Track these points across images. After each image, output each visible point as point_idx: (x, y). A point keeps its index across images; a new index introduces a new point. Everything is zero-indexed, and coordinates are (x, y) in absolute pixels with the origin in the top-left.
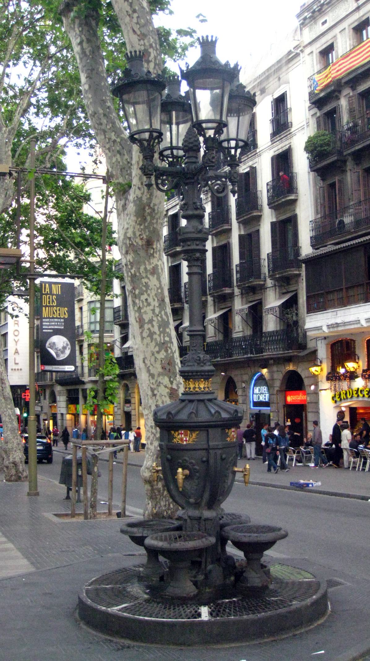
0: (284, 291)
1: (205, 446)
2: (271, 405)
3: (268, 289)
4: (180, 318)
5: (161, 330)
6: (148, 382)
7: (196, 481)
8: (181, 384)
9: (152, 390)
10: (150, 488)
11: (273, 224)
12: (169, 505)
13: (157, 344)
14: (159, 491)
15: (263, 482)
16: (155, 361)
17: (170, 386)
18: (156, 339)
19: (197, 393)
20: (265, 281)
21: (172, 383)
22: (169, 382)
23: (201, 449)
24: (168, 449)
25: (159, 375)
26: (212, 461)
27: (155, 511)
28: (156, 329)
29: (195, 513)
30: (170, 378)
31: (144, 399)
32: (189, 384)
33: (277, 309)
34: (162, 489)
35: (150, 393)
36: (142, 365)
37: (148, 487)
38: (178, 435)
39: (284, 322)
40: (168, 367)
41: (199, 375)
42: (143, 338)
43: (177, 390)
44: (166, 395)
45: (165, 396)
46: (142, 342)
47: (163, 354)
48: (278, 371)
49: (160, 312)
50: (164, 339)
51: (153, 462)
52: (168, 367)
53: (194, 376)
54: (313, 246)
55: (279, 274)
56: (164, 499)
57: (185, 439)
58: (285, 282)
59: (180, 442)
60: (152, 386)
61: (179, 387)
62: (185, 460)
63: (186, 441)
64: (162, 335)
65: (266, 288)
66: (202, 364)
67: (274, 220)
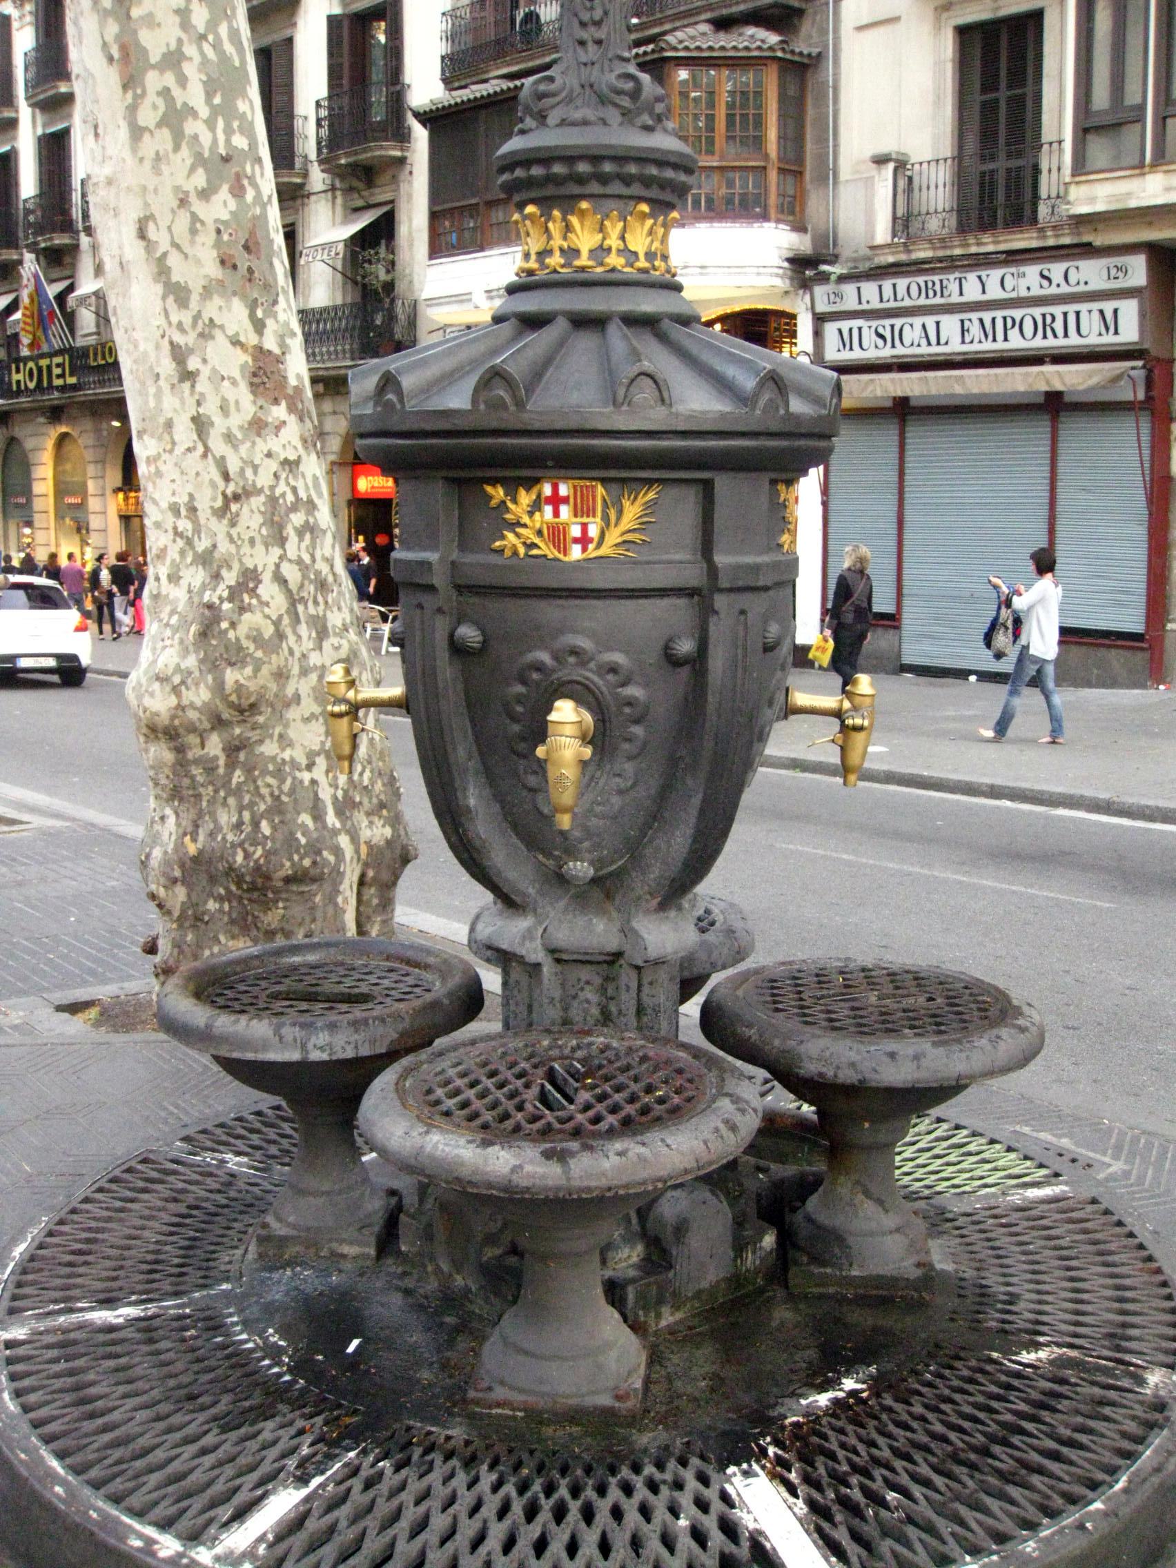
0: (360, 203)
1: (693, 575)
3: (313, 198)
4: (68, 273)
5: (217, 100)
6: (161, 321)
7: (629, 767)
8: (294, 334)
9: (179, 355)
10: (169, 757)
11: (333, 21)
12: (256, 825)
13: (199, 160)
14: (210, 770)
15: (967, 778)
16: (193, 232)
17: (252, 339)
18: (195, 137)
19: (612, 282)
20: (305, 175)
21: (259, 326)
22: (250, 328)
23: (663, 593)
24: (459, 588)
25: (207, 292)
26: (717, 662)
27: (192, 849)
28: (195, 95)
29: (596, 931)
30: (253, 306)
31: (143, 393)
32: (568, 228)
33: (341, 247)
34: (222, 762)
35: (167, 367)
36: (134, 251)
37: (161, 752)
38: (536, 507)
39: (355, 283)
40: (244, 261)
41: (627, 180)
42: (137, 132)
43: (279, 360)
44: (236, 374)
45: (234, 383)
46: (134, 150)
47: (221, 207)
48: (335, 413)
49: (212, 25)
50: (228, 141)
51: (185, 652)
52: (244, 261)
53: (604, 179)
54: (447, 81)
55: (347, 155)
56: (232, 801)
57: (576, 531)
58: (362, 177)
59: (546, 549)
60: (179, 339)
61: (285, 349)
62: (575, 652)
63: (584, 540)
64: (220, 124)
65: (308, 196)
66: (647, 119)
67: (337, 10)
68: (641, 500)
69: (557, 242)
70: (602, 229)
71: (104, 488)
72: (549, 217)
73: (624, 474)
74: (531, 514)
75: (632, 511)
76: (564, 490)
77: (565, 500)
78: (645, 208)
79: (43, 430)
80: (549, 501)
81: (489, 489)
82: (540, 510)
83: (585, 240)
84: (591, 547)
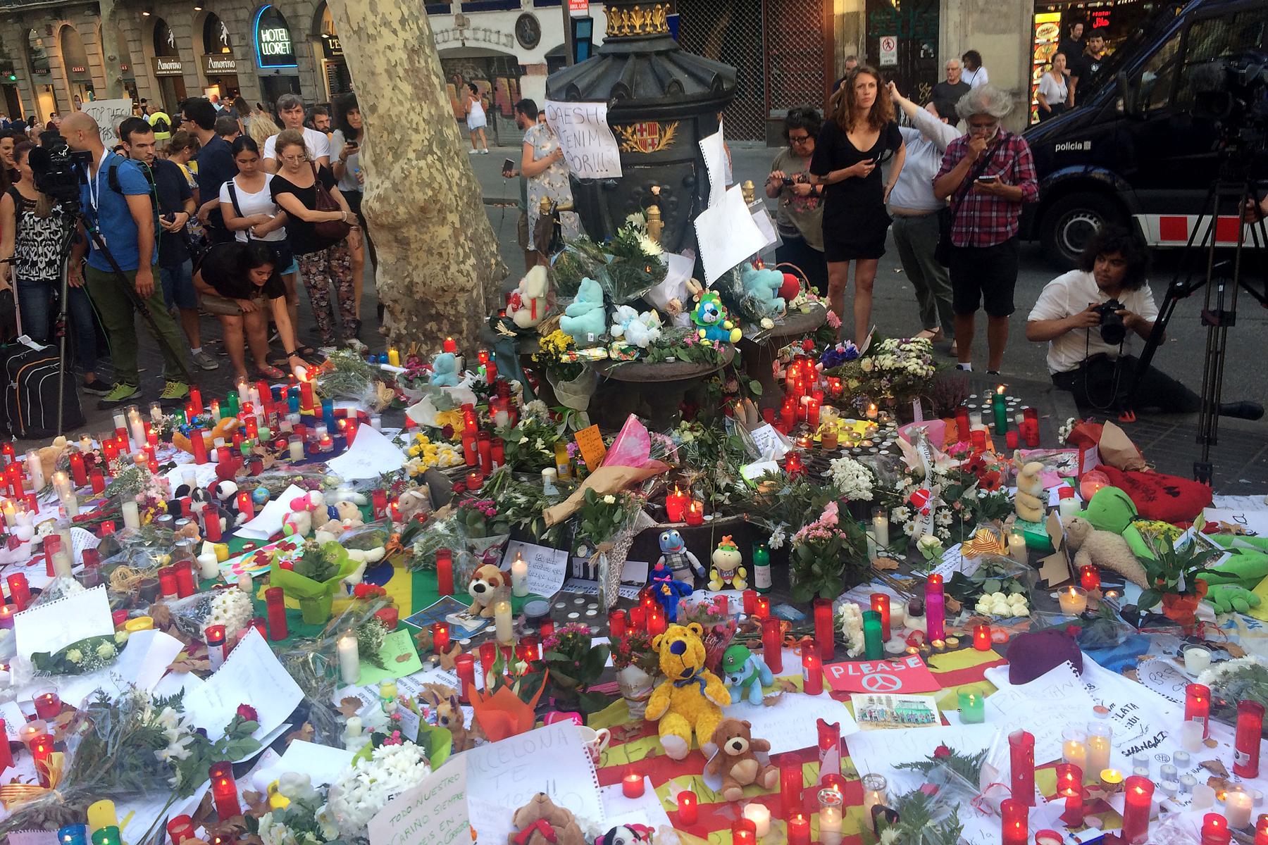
2: (298, 60)
19: (636, 39)
38: (634, 133)
63: (653, 145)
69: (626, 23)
70: (643, 16)
71: (143, 58)
75: (670, 133)
79: (91, 19)
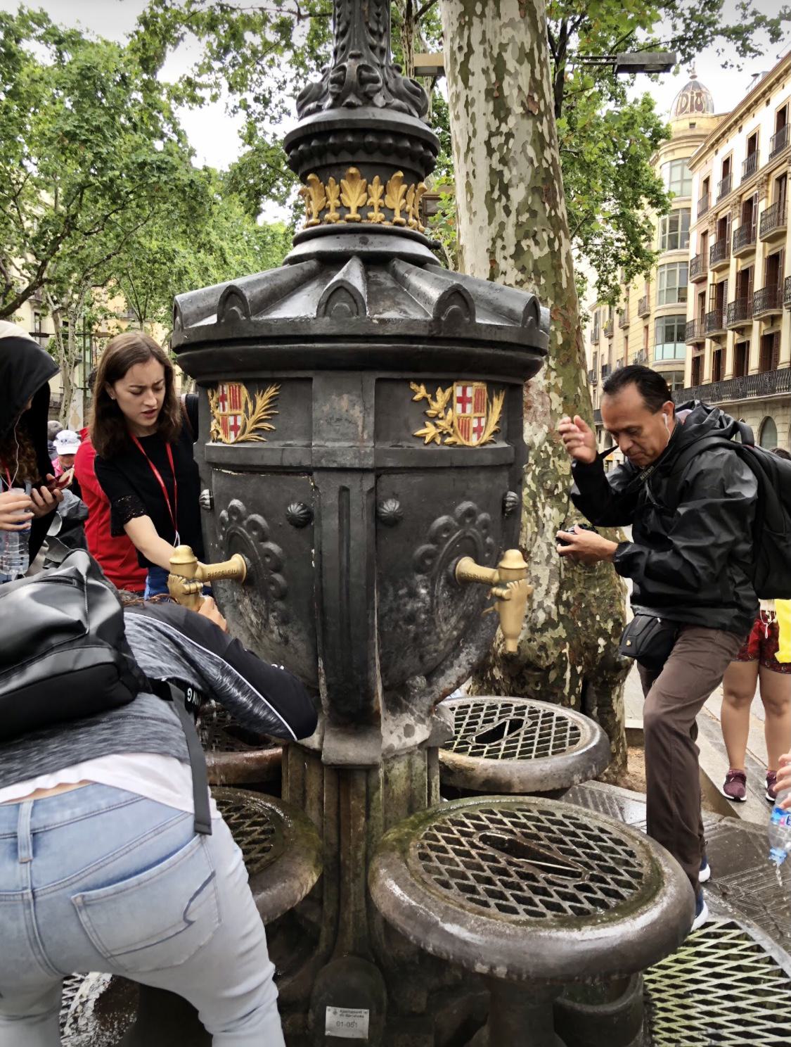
38: (449, 405)
63: (478, 430)
68: (266, 396)
69: (333, 202)
72: (326, 184)
73: (284, 375)
74: (446, 409)
75: (262, 402)
76: (470, 392)
77: (469, 400)
78: (353, 170)
80: (460, 400)
81: (414, 386)
82: (452, 406)
83: (354, 199)
84: (239, 433)
